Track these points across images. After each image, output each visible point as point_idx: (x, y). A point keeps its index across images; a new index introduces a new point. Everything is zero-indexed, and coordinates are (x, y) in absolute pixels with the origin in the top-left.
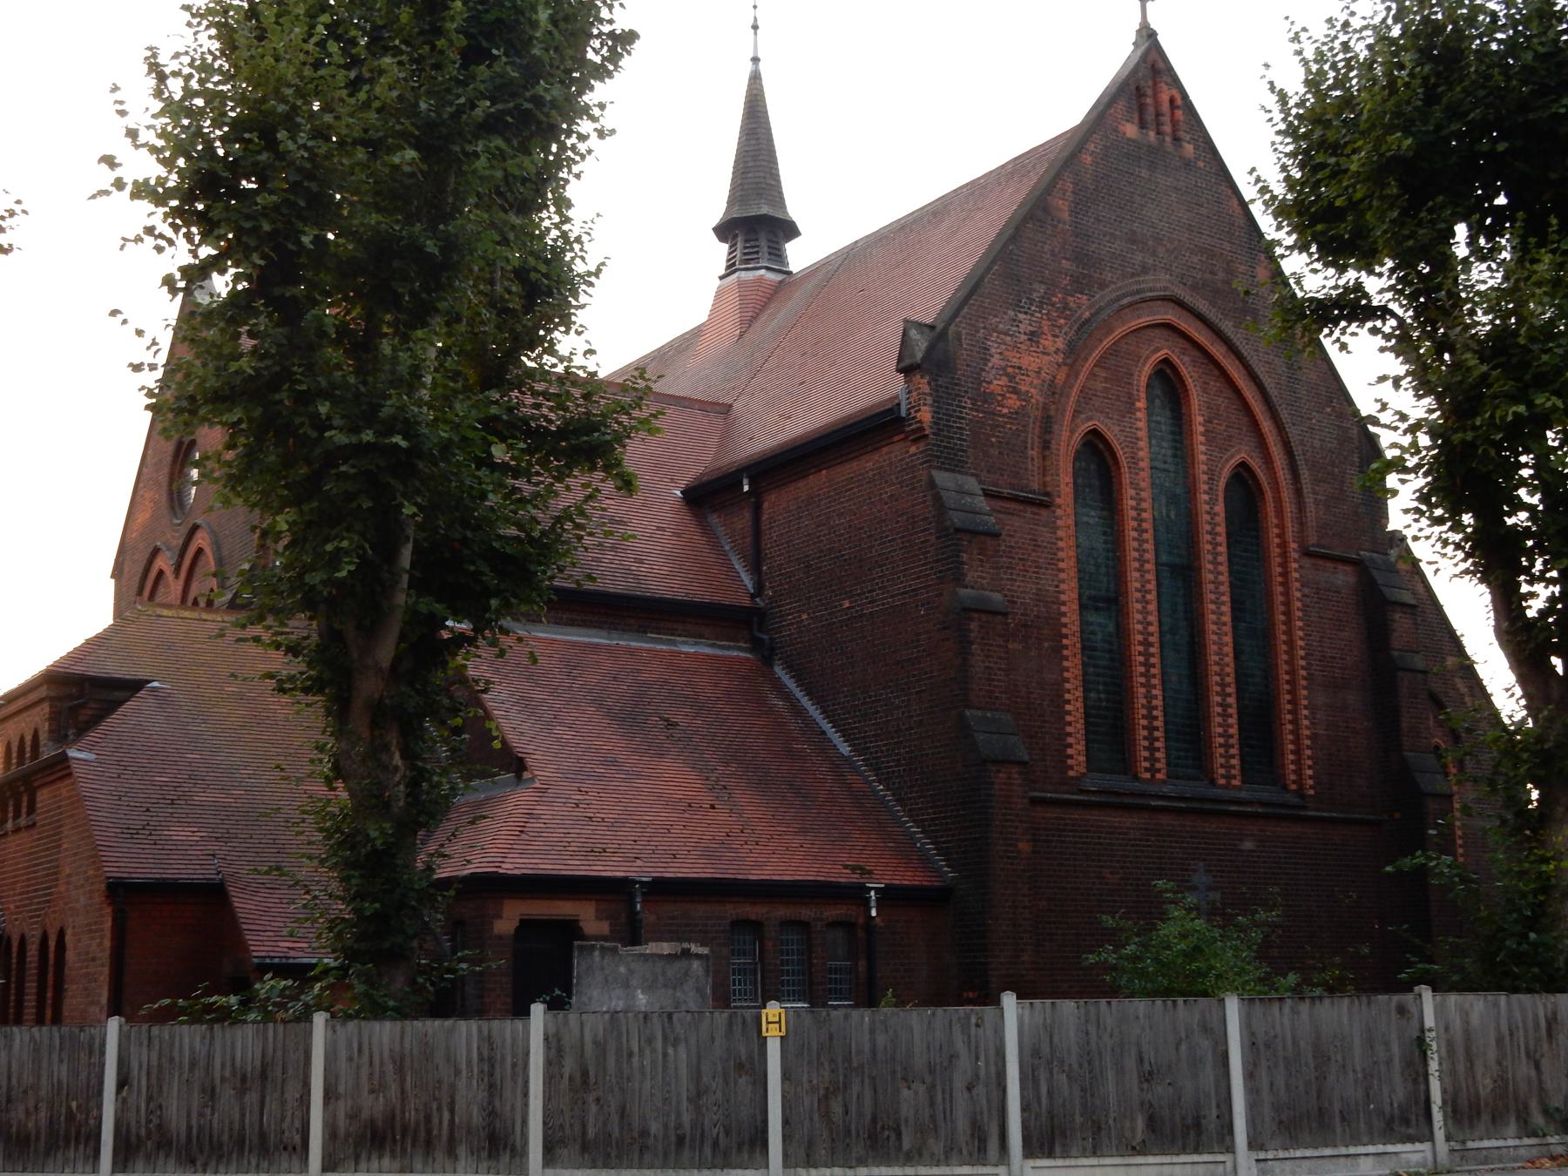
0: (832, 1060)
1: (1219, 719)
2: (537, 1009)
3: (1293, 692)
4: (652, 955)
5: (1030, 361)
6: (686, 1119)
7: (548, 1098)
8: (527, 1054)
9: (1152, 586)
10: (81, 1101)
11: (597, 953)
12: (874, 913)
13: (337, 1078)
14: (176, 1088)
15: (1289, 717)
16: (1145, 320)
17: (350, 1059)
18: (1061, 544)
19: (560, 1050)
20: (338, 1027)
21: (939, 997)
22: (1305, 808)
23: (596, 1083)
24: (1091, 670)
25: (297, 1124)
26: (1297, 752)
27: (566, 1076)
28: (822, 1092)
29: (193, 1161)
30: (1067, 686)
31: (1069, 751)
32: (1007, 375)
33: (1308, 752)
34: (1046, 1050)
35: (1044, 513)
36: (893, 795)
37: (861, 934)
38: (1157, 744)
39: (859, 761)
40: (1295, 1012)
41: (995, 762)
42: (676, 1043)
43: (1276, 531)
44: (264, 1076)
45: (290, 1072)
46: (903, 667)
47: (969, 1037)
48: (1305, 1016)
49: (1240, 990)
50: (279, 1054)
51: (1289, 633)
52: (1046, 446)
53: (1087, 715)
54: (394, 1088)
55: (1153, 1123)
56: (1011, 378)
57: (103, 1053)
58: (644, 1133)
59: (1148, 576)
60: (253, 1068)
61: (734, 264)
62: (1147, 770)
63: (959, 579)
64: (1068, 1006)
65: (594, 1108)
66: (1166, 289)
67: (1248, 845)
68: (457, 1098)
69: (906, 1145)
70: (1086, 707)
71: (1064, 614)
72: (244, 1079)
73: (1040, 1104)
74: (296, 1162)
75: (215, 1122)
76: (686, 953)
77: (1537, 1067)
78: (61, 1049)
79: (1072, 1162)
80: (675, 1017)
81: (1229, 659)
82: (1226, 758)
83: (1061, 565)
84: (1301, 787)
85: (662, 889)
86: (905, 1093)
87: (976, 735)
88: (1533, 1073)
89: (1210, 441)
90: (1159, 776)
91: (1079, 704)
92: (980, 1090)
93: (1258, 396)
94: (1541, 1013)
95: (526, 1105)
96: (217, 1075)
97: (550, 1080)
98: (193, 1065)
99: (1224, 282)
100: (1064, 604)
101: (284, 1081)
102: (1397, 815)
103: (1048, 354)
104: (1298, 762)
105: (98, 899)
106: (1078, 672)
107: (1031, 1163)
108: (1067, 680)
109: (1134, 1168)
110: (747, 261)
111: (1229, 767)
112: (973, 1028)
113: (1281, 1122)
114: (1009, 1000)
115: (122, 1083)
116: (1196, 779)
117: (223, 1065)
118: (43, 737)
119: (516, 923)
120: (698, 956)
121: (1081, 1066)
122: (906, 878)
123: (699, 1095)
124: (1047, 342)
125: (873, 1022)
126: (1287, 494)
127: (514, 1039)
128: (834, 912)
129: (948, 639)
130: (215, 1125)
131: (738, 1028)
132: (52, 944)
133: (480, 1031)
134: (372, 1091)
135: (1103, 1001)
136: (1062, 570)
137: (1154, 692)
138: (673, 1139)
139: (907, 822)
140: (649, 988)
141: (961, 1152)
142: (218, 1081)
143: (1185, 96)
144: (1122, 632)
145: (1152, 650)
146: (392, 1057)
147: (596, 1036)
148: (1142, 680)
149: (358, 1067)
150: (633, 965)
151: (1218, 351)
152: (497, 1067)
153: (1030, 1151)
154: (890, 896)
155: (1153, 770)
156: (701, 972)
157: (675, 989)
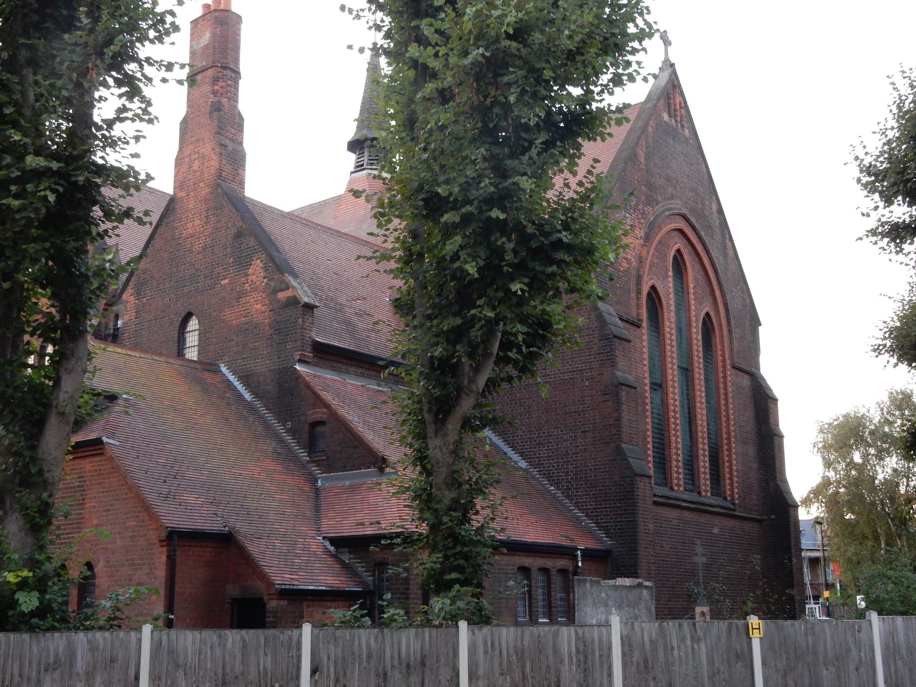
0: (786, 652)
4: (620, 586)
10: (281, 683)
11: (588, 584)
13: (477, 665)
14: (357, 673)
17: (486, 652)
19: (630, 646)
20: (476, 631)
22: (735, 510)
23: (653, 667)
27: (635, 663)
34: (891, 645)
35: (638, 330)
36: (562, 493)
41: (640, 475)
42: (698, 641)
44: (423, 664)
45: (443, 661)
46: (571, 416)
47: (855, 639)
54: (517, 674)
57: (299, 649)
60: (415, 659)
61: (363, 165)
63: (614, 365)
66: (680, 209)
68: (562, 678)
72: (408, 666)
76: (640, 585)
78: (265, 646)
84: (733, 499)
87: (629, 459)
89: (695, 299)
93: (714, 276)
96: (388, 664)
98: (369, 656)
99: (701, 209)
101: (438, 667)
102: (773, 517)
103: (637, 239)
110: (372, 164)
116: (692, 491)
117: (392, 657)
120: (646, 587)
121: (907, 656)
122: (591, 545)
125: (806, 628)
126: (725, 332)
127: (600, 640)
128: (559, 563)
129: (608, 401)
131: (734, 632)
133: (577, 634)
134: (502, 674)
139: (574, 510)
142: (389, 668)
143: (685, 102)
144: (664, 403)
146: (516, 651)
147: (651, 637)
149: (492, 657)
150: (609, 592)
151: (699, 247)
152: (590, 657)
156: (648, 597)
157: (634, 608)
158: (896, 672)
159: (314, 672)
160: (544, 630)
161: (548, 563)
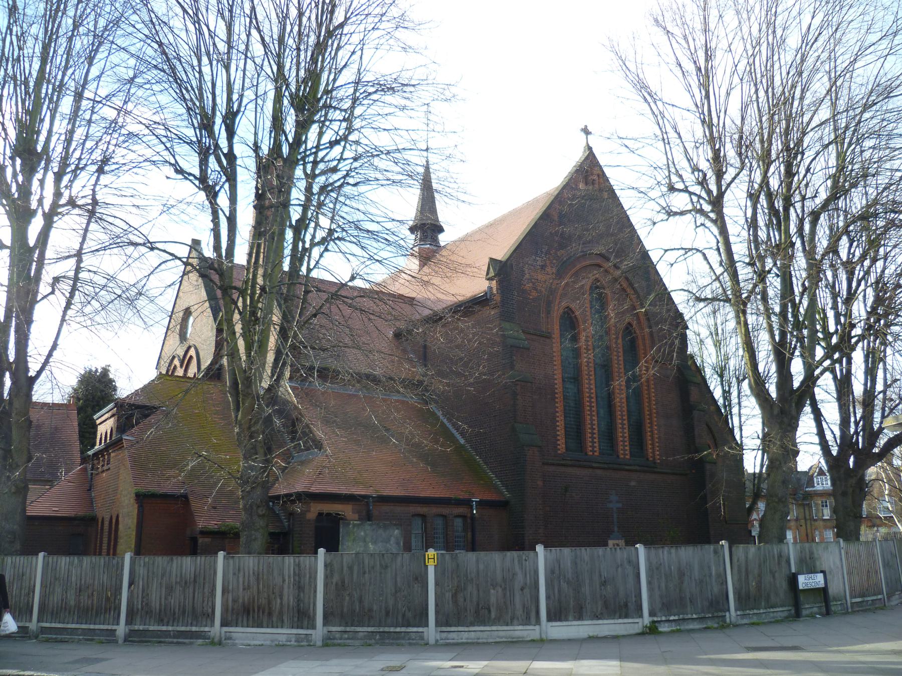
0: (458, 577)
1: (620, 430)
2: (322, 551)
3: (650, 419)
5: (541, 277)
6: (391, 602)
7: (326, 593)
8: (316, 572)
9: (592, 373)
12: (475, 512)
15: (649, 429)
16: (588, 262)
17: (234, 574)
18: (555, 354)
21: (506, 547)
24: (567, 408)
25: (210, 604)
26: (653, 444)
27: (334, 583)
28: (454, 591)
29: (162, 620)
30: (558, 414)
31: (558, 442)
32: (532, 282)
33: (657, 444)
35: (548, 340)
37: (469, 521)
38: (595, 440)
39: (468, 446)
40: (670, 553)
43: (643, 352)
44: (195, 581)
48: (673, 555)
49: (646, 543)
50: (202, 571)
51: (649, 394)
52: (548, 312)
53: (565, 427)
55: (606, 605)
56: (534, 284)
57: (122, 570)
58: (370, 610)
59: (591, 369)
62: (591, 451)
64: (566, 551)
65: (347, 598)
67: (633, 483)
69: (493, 615)
70: (565, 424)
71: (556, 384)
73: (554, 596)
74: (209, 622)
75: (173, 601)
77: (774, 577)
79: (569, 623)
80: (385, 556)
81: (624, 405)
82: (624, 448)
83: (555, 363)
84: (654, 459)
85: (384, 500)
86: (492, 591)
88: (772, 580)
90: (596, 454)
91: (563, 423)
92: (527, 591)
94: (776, 553)
95: (315, 596)
97: (326, 585)
98: (163, 575)
100: (556, 379)
102: (694, 471)
104: (653, 448)
105: (132, 501)
106: (562, 408)
107: (550, 624)
108: (557, 412)
109: (55, 353)
111: (625, 450)
112: (524, 562)
113: (663, 603)
114: (540, 548)
115: (131, 584)
118: (114, 432)
119: (316, 514)
122: (488, 497)
123: (396, 592)
124: (548, 269)
130: (172, 604)
132: (114, 521)
133: (294, 562)
135: (583, 549)
136: (555, 365)
137: (594, 418)
138: (384, 612)
140: (375, 543)
141: (518, 619)
144: (580, 392)
145: (593, 400)
148: (589, 413)
153: (550, 619)
154: (481, 504)
155: (593, 451)
158: (559, 591)
159: (130, 585)
160: (274, 559)
161: (445, 511)
